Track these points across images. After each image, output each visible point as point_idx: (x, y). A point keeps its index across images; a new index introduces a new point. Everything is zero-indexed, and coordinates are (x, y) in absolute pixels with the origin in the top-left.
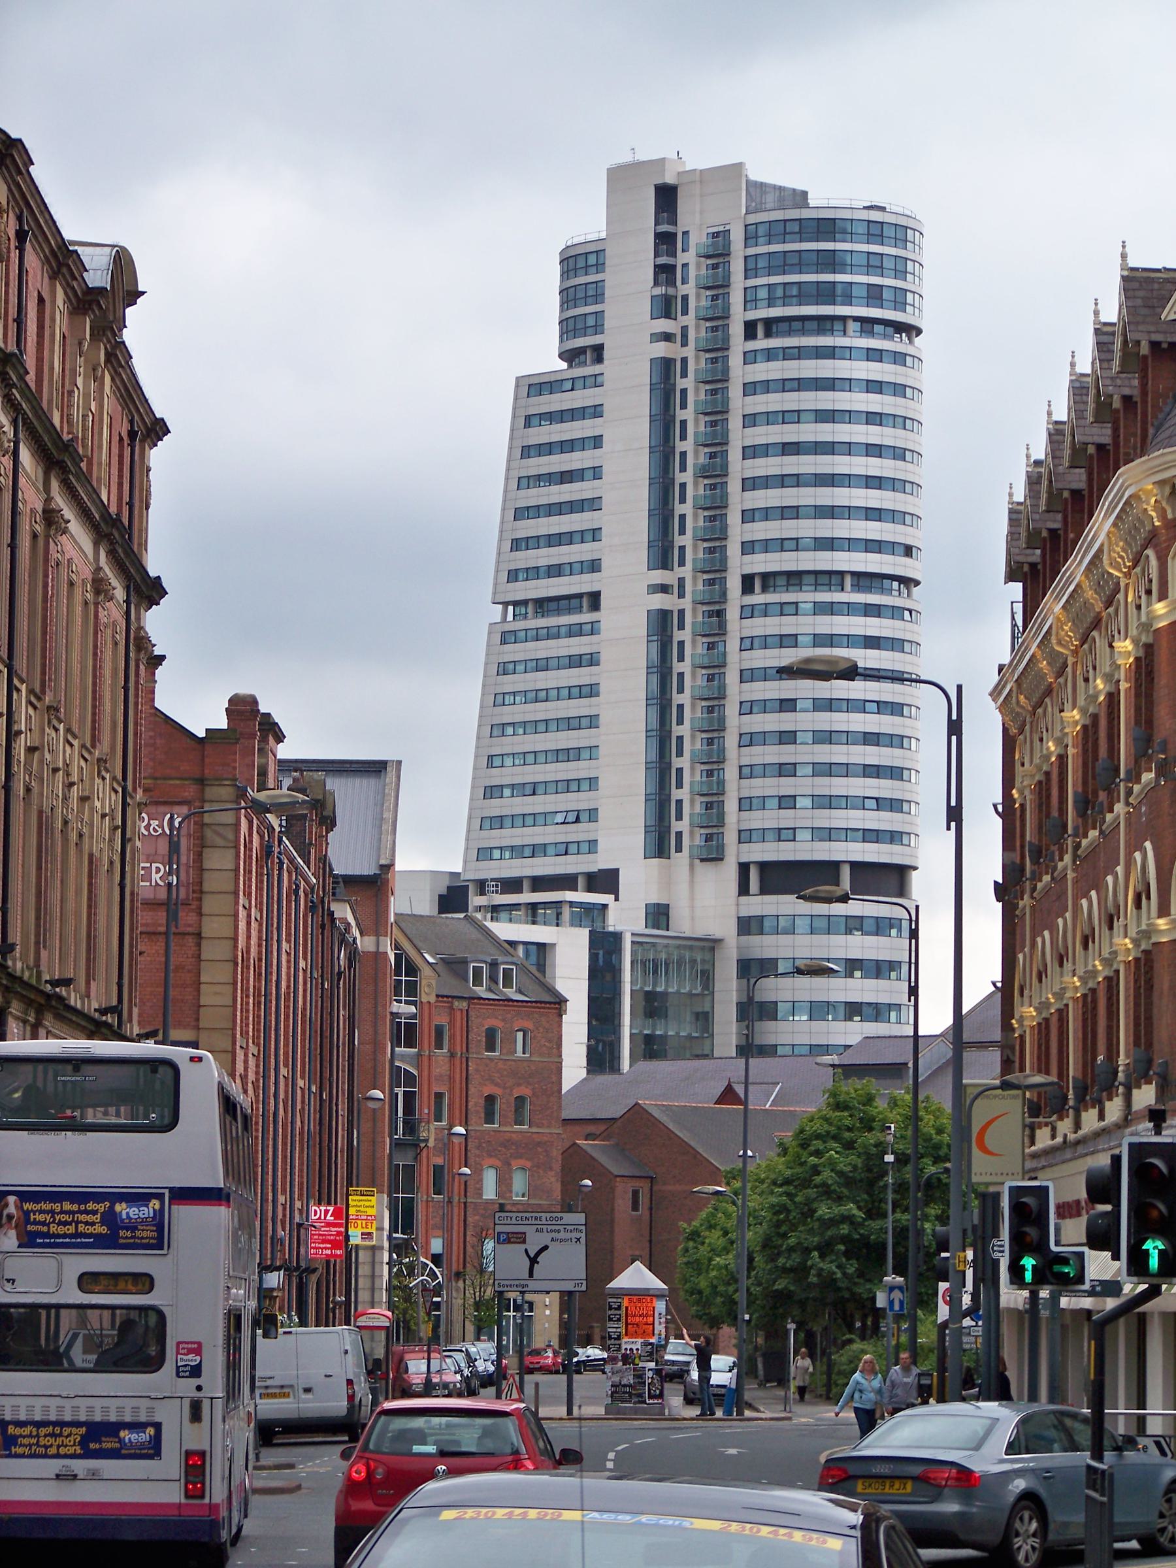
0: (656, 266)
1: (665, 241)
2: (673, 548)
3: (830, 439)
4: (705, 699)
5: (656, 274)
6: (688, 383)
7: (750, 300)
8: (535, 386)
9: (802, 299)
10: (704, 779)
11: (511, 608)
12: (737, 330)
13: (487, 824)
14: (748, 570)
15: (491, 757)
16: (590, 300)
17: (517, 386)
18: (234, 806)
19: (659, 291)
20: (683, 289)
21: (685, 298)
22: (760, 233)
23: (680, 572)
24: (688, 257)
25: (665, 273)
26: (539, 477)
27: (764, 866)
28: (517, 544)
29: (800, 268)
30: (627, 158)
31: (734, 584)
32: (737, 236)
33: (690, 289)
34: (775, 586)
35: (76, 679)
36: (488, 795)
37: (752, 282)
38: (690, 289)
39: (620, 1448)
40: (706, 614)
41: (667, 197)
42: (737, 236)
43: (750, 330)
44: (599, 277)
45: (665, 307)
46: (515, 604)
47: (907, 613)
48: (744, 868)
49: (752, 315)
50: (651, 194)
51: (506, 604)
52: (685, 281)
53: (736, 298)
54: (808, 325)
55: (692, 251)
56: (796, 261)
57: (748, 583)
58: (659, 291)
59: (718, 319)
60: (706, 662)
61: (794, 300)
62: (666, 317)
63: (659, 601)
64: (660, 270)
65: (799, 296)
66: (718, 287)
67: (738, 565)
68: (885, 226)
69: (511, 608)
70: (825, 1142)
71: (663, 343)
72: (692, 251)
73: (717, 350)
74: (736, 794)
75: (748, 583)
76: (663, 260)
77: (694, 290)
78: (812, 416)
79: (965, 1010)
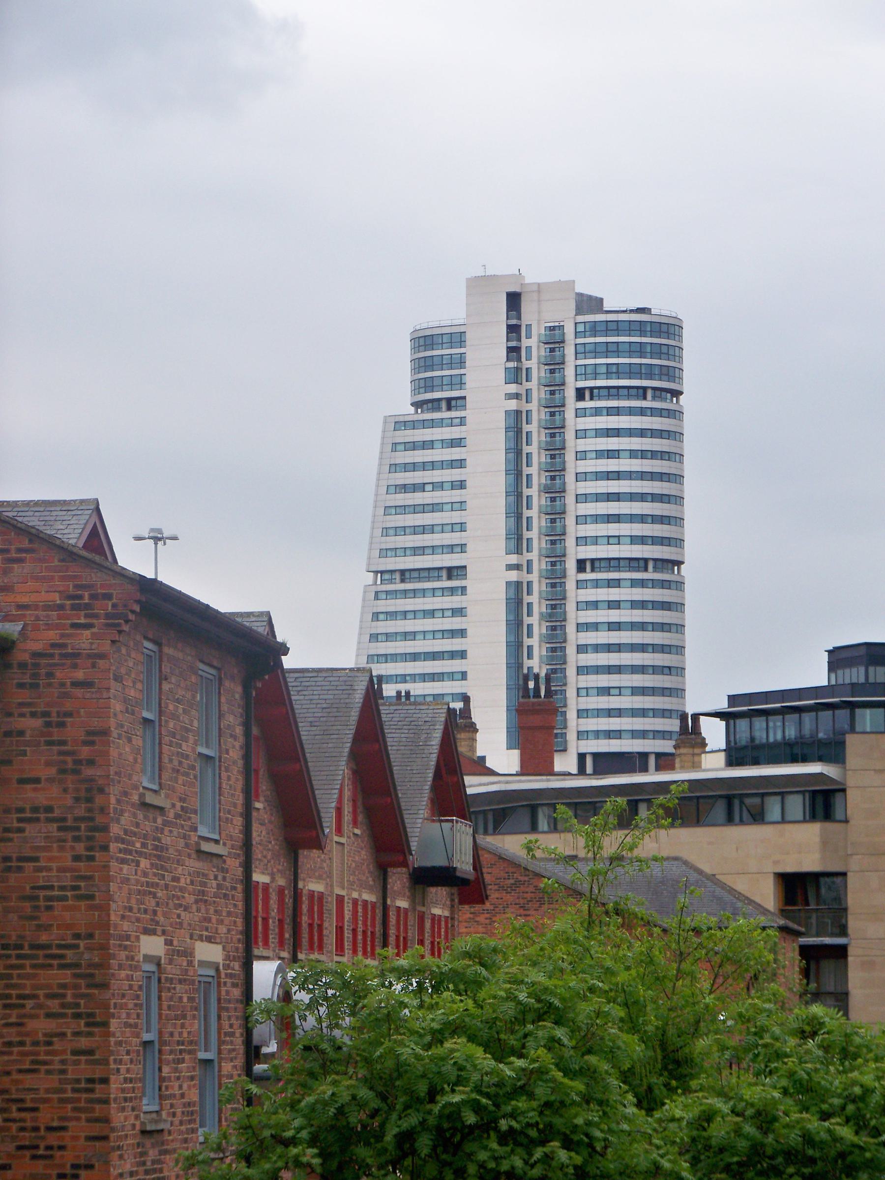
0: (508, 348)
1: (513, 330)
2: (522, 475)
3: (632, 417)
6: (533, 428)
7: (581, 372)
8: (402, 424)
9: (619, 375)
10: (549, 503)
12: (570, 394)
13: (392, 490)
14: (581, 556)
15: (377, 593)
17: (385, 422)
19: (511, 365)
21: (529, 349)
22: (588, 371)
23: (528, 385)
24: (532, 343)
25: (513, 352)
26: (404, 486)
27: (596, 756)
28: (386, 532)
29: (617, 353)
31: (571, 566)
33: (533, 364)
34: (600, 568)
36: (384, 534)
38: (533, 385)
40: (549, 650)
41: (514, 300)
43: (580, 394)
45: (516, 375)
46: (382, 572)
47: (678, 456)
48: (582, 757)
49: (581, 384)
51: (376, 572)
52: (529, 336)
53: (570, 372)
54: (621, 391)
55: (535, 423)
57: (581, 565)
58: (511, 365)
59: (555, 387)
60: (549, 510)
61: (614, 375)
62: (517, 383)
63: (513, 576)
64: (510, 350)
65: (617, 373)
66: (555, 365)
67: (574, 553)
71: (515, 401)
72: (535, 423)
73: (555, 408)
74: (574, 685)
75: (581, 565)
76: (513, 344)
77: (537, 451)
78: (628, 540)
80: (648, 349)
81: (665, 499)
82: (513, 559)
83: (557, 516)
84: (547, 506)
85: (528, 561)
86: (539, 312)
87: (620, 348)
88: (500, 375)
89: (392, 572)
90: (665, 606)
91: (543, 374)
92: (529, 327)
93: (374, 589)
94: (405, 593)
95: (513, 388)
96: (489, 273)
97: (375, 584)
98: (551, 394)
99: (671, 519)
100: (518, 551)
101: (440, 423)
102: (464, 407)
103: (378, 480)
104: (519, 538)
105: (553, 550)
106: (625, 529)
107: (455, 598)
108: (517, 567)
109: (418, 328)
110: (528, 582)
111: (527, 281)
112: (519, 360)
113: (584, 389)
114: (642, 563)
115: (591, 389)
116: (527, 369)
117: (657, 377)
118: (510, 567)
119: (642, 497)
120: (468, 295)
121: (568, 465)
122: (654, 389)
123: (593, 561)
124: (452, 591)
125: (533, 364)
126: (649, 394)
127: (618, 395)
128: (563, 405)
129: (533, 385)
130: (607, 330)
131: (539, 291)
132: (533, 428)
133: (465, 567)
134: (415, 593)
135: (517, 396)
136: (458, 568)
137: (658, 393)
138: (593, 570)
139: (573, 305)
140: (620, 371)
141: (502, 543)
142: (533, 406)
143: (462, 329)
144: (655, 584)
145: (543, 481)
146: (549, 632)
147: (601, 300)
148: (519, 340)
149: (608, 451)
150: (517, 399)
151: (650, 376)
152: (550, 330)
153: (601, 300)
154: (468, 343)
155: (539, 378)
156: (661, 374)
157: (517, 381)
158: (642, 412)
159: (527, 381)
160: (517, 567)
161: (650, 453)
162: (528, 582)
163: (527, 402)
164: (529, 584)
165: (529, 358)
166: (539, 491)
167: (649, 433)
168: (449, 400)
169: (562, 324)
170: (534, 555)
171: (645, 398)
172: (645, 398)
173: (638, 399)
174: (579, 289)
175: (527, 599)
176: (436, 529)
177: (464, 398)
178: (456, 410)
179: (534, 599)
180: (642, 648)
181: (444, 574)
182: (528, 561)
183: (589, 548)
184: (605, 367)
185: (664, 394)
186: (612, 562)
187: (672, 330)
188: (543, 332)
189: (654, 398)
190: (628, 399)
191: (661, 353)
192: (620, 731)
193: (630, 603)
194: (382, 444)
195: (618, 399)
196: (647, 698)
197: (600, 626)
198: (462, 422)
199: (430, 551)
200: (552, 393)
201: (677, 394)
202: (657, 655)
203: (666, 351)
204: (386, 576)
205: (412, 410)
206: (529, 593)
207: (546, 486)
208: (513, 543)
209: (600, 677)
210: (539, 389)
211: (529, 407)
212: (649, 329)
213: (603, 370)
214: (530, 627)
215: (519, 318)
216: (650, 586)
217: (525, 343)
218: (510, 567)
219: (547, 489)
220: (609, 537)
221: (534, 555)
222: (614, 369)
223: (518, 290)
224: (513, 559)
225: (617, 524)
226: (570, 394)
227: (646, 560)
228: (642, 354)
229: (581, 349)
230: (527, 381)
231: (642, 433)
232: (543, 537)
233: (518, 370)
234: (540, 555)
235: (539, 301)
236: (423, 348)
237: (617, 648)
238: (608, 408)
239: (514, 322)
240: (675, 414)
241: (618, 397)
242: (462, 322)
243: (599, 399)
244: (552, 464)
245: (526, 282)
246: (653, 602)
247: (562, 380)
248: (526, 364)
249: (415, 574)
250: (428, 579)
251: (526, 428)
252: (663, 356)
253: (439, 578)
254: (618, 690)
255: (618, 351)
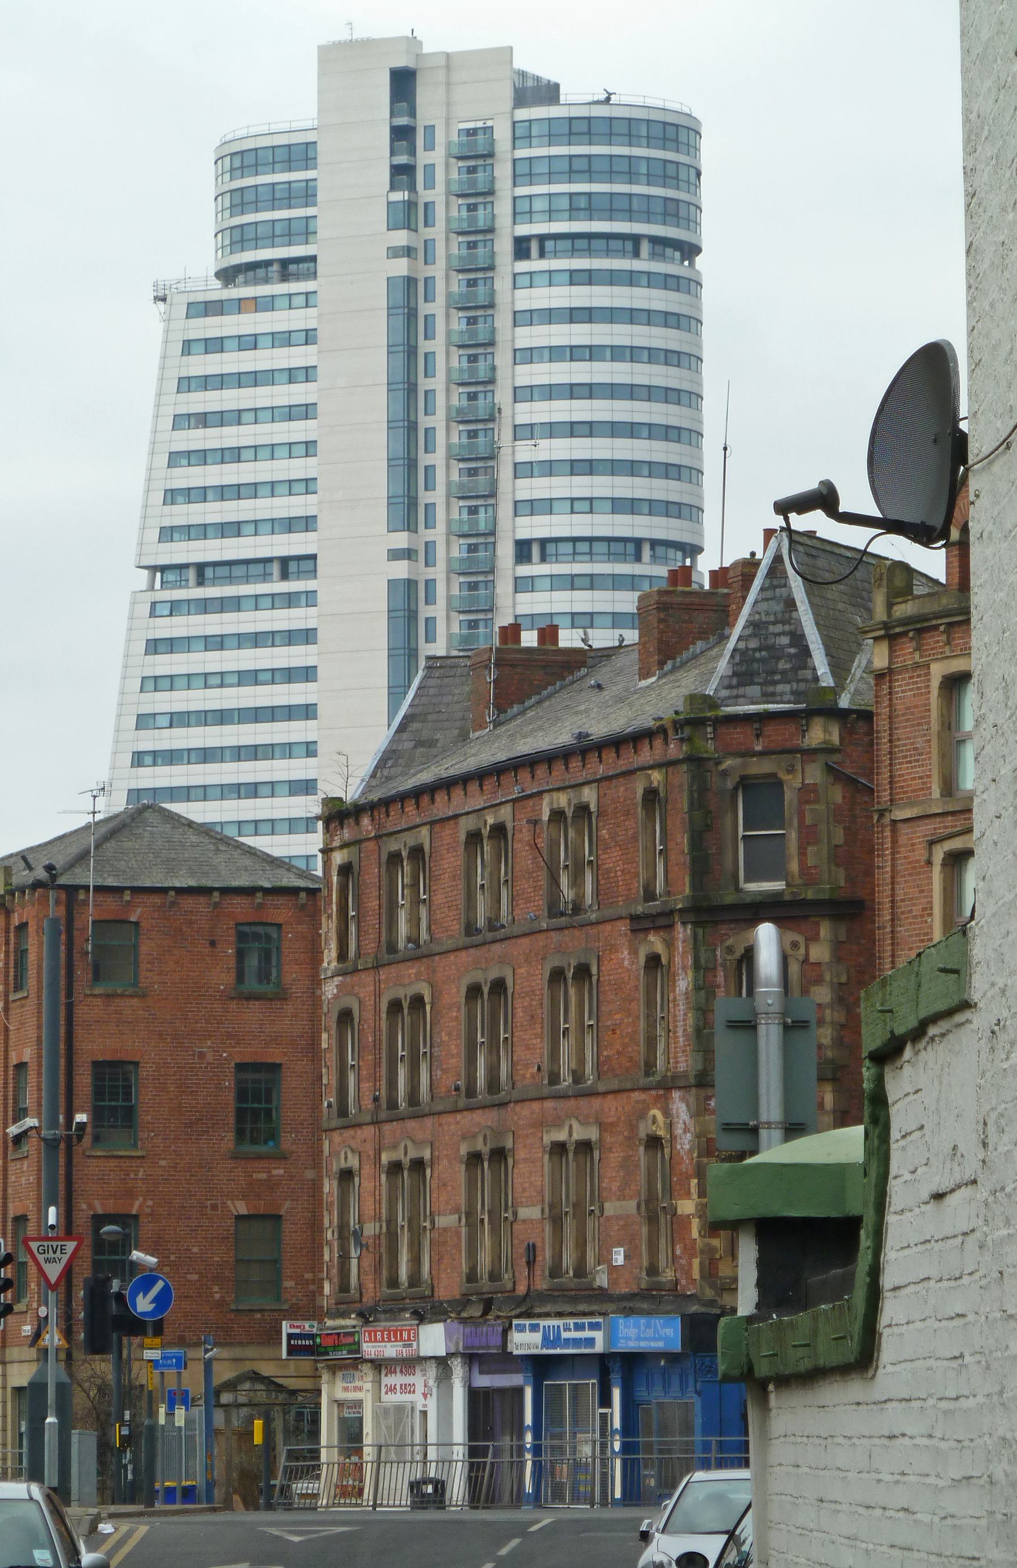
3: (615, 288)
4: (463, 612)
5: (393, 175)
11: (158, 574)
12: (504, 247)
13: (150, 684)
14: (523, 534)
15: (154, 604)
16: (277, 166)
18: (408, 1465)
19: (398, 196)
20: (429, 535)
21: (430, 168)
23: (427, 233)
30: (344, 36)
32: (502, 135)
33: (436, 195)
35: (399, 1486)
37: (522, 191)
38: (438, 232)
39: (504, 1551)
42: (502, 135)
44: (310, 211)
50: (385, 80)
51: (153, 569)
52: (430, 146)
54: (597, 244)
55: (440, 299)
56: (585, 129)
58: (398, 196)
61: (582, 213)
62: (409, 228)
64: (397, 170)
68: (682, 393)
69: (158, 574)
70: (631, 706)
75: (523, 550)
76: (402, 159)
78: (608, 506)
79: (875, 512)
80: (643, 170)
81: (672, 282)
82: (401, 540)
83: (480, 388)
84: (461, 521)
85: (426, 543)
86: (448, 104)
87: (595, 167)
88: (380, 215)
89: (182, 567)
90: (668, 433)
91: (455, 176)
92: (430, 129)
93: (150, 597)
94: (205, 606)
95: (401, 238)
96: (358, 35)
97: (152, 588)
98: (469, 248)
99: (682, 319)
100: (410, 526)
101: (268, 304)
102: (313, 573)
103: (158, 406)
104: (412, 503)
105: (472, 220)
106: (601, 486)
107: (294, 612)
108: (408, 554)
109: (229, 138)
110: (427, 582)
111: (426, 50)
112: (412, 188)
113: (527, 239)
114: (631, 548)
115: (542, 238)
116: (426, 205)
117: (660, 218)
118: (395, 555)
119: (631, 392)
120: (322, 74)
121: (500, 374)
122: (655, 240)
123: (544, 542)
124: (290, 600)
125: (436, 195)
126: (645, 247)
127: (591, 553)
128: (491, 268)
129: (438, 232)
130: (570, 134)
131: (448, 67)
132: (437, 308)
133: (313, 557)
134: (223, 605)
135: (409, 252)
136: (299, 558)
137: (659, 249)
138: (543, 559)
139: (508, 93)
140: (594, 168)
141: (382, 512)
142: (439, 572)
143: (311, 137)
144: (651, 280)
145: (455, 402)
146: (465, 631)
147: (557, 86)
148: (412, 152)
149: (572, 347)
150: (409, 558)
151: (648, 217)
152: (470, 475)
153: (557, 86)
154: (320, 160)
155: (448, 182)
156: (665, 214)
157: (409, 225)
158: (631, 279)
159: (426, 225)
160: (408, 554)
161: (646, 353)
162: (427, 582)
163: (427, 565)
164: (430, 584)
165: (430, 184)
166: (448, 420)
167: (644, 393)
168: (285, 263)
169: (489, 123)
170: (438, 534)
171: (638, 558)
172: (636, 254)
173: (624, 257)
174: (519, 64)
175: (425, 611)
176: (262, 790)
177: (313, 259)
178: (298, 579)
179: (438, 610)
180: (631, 392)
181: (276, 568)
182: (426, 543)
183: (537, 519)
184: (567, 199)
185: (669, 251)
186: (578, 544)
187: (683, 137)
188: (455, 138)
189: (653, 256)
190: (607, 256)
191: (665, 176)
192: (592, 614)
193: (610, 617)
194: (161, 379)
195: (590, 257)
196: (638, 405)
197: (556, 505)
198: (310, 598)
199: (250, 529)
200: (472, 246)
201: (695, 250)
202: (655, 293)
203: (674, 137)
204: (171, 576)
205: (218, 284)
206: (430, 600)
207: (461, 486)
208: (401, 511)
209: (555, 328)
210: (447, 239)
211: (430, 573)
212: (644, 133)
213: (565, 203)
214: (430, 622)
215: (412, 113)
216: (646, 510)
217: (423, 158)
218: (395, 555)
219: (459, 417)
220: (573, 500)
221: (438, 534)
222: (583, 203)
223: (411, 65)
224: (401, 540)
225: (588, 287)
226: (504, 247)
227: (638, 542)
228: (631, 177)
229: (523, 206)
230: (426, 225)
231: (632, 468)
232: (454, 387)
233: (410, 206)
234: (448, 193)
235: (448, 84)
236: (239, 172)
237: (586, 391)
238: (572, 272)
239: (403, 121)
240: (690, 285)
241: (590, 252)
242: (309, 124)
243: (555, 257)
244: (471, 447)
245: (425, 51)
246: (650, 463)
247: (489, 261)
248: (425, 195)
249: (224, 571)
250: (247, 579)
251: (424, 309)
252: (668, 144)
253: (266, 577)
254: (587, 503)
255: (590, 171)
